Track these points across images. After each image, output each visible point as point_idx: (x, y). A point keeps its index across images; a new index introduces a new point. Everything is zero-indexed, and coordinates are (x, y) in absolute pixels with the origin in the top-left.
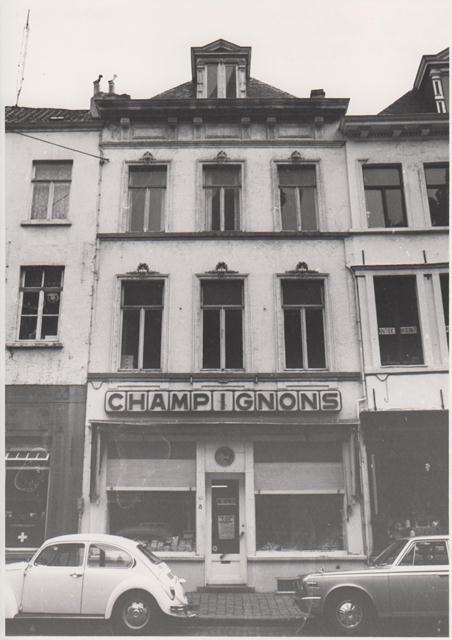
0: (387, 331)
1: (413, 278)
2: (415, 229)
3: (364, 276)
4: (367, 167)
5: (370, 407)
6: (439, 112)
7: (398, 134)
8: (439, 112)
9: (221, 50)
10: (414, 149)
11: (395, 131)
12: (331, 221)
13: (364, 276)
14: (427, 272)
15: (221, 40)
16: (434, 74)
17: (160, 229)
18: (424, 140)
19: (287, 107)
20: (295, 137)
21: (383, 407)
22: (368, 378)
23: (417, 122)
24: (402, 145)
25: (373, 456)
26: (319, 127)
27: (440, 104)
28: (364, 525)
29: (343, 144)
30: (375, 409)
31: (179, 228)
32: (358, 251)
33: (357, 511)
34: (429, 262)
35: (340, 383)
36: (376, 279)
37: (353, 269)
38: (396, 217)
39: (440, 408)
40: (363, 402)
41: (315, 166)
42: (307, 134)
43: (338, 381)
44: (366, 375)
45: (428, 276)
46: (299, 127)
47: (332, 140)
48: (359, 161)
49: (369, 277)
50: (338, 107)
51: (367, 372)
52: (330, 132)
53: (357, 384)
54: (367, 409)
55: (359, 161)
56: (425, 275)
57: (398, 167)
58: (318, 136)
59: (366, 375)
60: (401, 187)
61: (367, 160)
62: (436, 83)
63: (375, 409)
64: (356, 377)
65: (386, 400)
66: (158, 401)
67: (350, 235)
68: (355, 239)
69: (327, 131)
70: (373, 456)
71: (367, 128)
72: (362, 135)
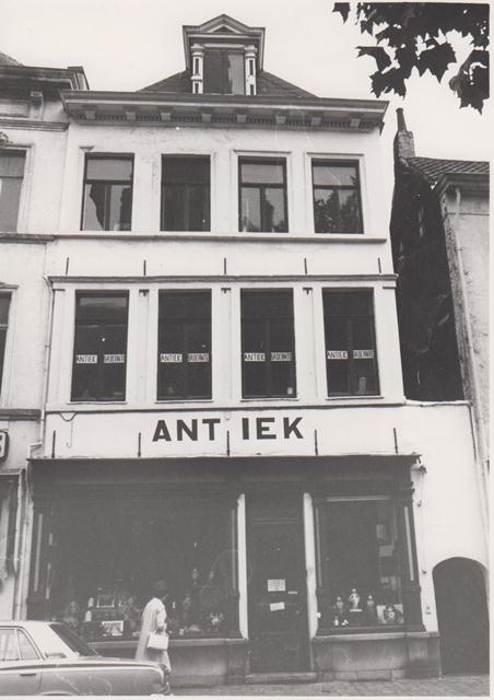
0: (254, 357)
1: (290, 292)
2: (370, 237)
3: (63, 290)
4: (91, 157)
5: (47, 453)
6: (194, 91)
7: (318, 123)
8: (194, 91)
9: (224, 30)
10: (151, 137)
11: (239, 116)
12: (28, 223)
13: (63, 290)
14: (144, 286)
15: (224, 18)
16: (196, 50)
17: (15, 227)
18: (166, 127)
19: (7, 77)
20: (6, 115)
21: (63, 453)
22: (49, 416)
23: (230, 105)
24: (138, 131)
25: (41, 516)
26: (37, 104)
27: (197, 85)
28: (15, 606)
29: (66, 127)
30: (53, 456)
31: (34, 230)
32: (55, 259)
33: (9, 586)
34: (229, 274)
35: (12, 423)
36: (326, 292)
37: (51, 280)
38: (277, 219)
39: (314, 454)
40: (39, 446)
41: (25, 152)
42: (21, 113)
43: (9, 420)
44: (47, 413)
45: (308, 290)
46: (13, 103)
47: (55, 120)
48: (82, 148)
49: (71, 289)
50: (61, 80)
51: (48, 410)
52: (53, 112)
53: (34, 424)
54: (42, 457)
55: (82, 148)
56: (304, 289)
57: (130, 158)
58: (34, 115)
59: (47, 413)
60: (284, 186)
61: (91, 148)
62: (251, 62)
63: (53, 456)
64: (34, 416)
65: (69, 446)
66: (162, 434)
67: (55, 238)
68: (61, 243)
69: (47, 111)
70: (41, 516)
71: (93, 107)
72: (313, 123)
